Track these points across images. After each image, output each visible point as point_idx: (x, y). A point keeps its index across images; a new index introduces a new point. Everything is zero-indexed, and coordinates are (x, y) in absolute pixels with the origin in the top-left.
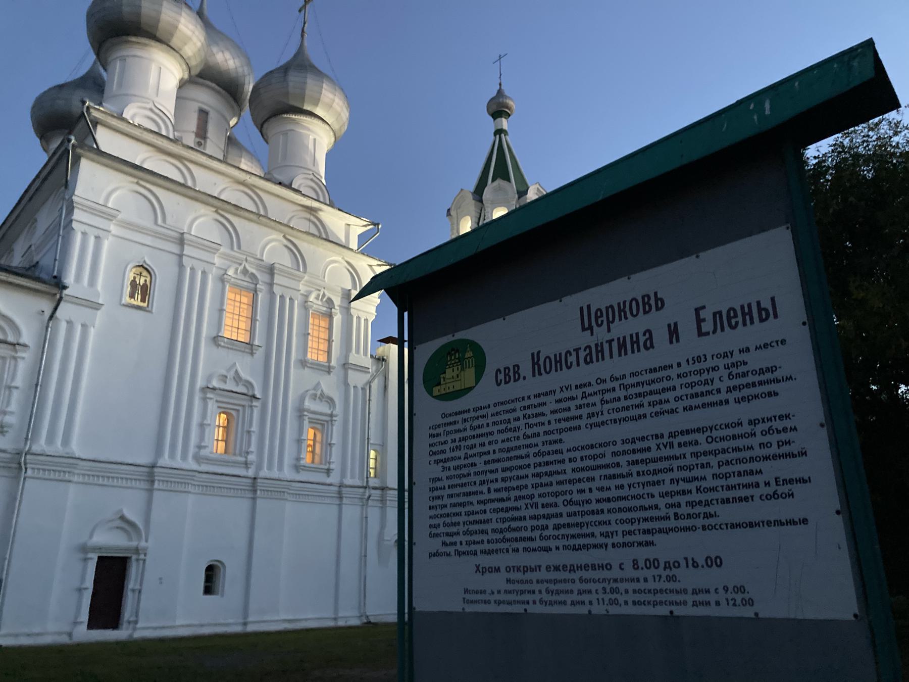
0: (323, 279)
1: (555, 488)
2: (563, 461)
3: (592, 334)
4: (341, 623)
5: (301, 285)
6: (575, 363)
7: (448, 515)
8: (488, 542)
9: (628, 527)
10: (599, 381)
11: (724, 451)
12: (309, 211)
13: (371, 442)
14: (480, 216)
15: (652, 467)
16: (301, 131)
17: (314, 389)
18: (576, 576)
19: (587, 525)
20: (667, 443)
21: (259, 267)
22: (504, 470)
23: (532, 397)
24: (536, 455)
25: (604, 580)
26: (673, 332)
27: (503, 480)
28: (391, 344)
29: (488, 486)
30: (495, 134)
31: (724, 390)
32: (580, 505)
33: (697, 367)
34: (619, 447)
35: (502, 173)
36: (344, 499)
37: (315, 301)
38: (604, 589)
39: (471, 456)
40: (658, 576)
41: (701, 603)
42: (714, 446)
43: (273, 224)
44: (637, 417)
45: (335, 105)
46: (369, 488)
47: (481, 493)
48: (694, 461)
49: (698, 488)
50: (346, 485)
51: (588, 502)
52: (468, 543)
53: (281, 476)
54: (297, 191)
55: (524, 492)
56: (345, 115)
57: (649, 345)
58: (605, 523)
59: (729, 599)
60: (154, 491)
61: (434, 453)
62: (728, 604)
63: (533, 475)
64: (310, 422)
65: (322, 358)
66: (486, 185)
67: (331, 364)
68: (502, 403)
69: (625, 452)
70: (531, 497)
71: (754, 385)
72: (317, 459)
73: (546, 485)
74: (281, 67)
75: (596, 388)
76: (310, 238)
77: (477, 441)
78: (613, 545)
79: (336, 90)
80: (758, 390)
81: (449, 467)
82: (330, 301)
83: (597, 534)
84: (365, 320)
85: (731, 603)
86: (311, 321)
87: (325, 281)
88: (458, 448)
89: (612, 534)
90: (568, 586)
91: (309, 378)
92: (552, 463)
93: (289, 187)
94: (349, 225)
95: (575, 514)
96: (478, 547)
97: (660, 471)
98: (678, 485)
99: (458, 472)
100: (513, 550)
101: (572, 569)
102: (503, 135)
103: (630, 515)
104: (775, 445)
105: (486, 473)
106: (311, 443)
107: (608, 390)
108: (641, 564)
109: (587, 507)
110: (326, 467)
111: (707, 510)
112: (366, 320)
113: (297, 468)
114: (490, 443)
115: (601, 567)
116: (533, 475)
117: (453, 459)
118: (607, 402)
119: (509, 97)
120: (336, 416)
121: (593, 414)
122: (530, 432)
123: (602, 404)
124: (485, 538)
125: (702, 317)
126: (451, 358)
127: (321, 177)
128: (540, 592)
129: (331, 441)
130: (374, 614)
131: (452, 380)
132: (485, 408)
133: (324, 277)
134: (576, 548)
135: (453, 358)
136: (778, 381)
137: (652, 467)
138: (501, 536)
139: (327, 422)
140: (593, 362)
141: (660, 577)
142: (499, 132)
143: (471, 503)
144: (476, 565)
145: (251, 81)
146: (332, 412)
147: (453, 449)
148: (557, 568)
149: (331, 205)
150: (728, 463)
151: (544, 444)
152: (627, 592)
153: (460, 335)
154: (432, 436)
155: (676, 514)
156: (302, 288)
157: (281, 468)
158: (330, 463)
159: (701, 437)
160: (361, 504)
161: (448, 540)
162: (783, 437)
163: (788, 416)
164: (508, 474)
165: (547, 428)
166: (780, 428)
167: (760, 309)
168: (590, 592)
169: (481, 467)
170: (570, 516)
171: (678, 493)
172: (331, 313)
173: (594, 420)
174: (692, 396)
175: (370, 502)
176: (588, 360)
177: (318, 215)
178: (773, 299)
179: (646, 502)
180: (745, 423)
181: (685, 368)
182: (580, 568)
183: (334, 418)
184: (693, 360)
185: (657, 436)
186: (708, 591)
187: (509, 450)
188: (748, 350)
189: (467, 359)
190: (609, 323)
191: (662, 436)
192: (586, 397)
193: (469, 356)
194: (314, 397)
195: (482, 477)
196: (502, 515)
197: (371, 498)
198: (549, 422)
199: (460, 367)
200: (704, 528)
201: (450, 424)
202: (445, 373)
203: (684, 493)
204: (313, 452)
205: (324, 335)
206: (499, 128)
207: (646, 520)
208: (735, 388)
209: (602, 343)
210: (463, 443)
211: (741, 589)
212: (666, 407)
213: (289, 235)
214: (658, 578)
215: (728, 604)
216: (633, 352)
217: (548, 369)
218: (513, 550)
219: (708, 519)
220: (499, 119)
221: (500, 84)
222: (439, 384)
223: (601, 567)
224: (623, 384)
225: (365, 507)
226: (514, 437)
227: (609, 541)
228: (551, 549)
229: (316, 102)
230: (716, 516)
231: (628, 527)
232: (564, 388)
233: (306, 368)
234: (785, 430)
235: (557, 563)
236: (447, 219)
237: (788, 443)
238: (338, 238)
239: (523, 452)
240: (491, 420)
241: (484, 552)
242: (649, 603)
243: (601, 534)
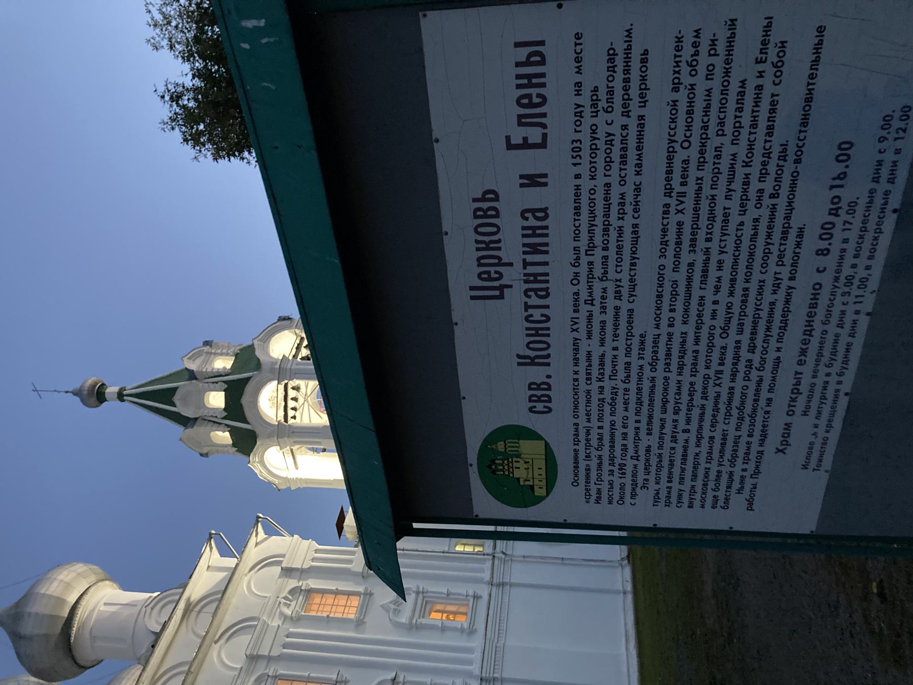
0: (268, 599)
1: (702, 347)
2: (670, 335)
3: (510, 286)
4: (629, 587)
5: (273, 624)
6: (545, 311)
7: (705, 485)
8: (750, 436)
9: (773, 258)
10: (575, 282)
11: (705, 128)
12: (189, 612)
13: (446, 549)
14: (211, 421)
15: (703, 222)
16: (93, 619)
17: (388, 611)
18: (817, 326)
19: (759, 310)
20: (677, 200)
21: (249, 673)
22: (664, 411)
23: (576, 369)
24: (653, 369)
25: (833, 294)
26: (532, 181)
27: (676, 412)
28: (345, 524)
29: (681, 432)
30: (123, 401)
31: (625, 121)
32: (730, 318)
33: (586, 152)
34: (669, 261)
35: (167, 396)
36: (504, 580)
37: (292, 607)
38: (843, 294)
39: (636, 452)
40: (844, 225)
41: (892, 172)
42: (695, 140)
43: (200, 655)
44: (634, 236)
45: (67, 579)
46: (494, 553)
47: (687, 441)
48: (709, 167)
49: (744, 164)
50: (491, 578)
51: (729, 307)
52: (746, 461)
53: (480, 650)
54: (165, 626)
55: (699, 387)
56: (80, 567)
57: (542, 213)
58: (761, 287)
59: (897, 136)
60: (503, 676)
61: (622, 498)
62: (903, 138)
63: (680, 374)
64: (423, 617)
65: (355, 601)
66: (179, 413)
67: (363, 592)
68: (576, 407)
69: (677, 255)
70: (706, 378)
71: (627, 81)
72: (462, 610)
73: (696, 358)
74: (13, 642)
75: (583, 288)
76: (220, 612)
77: (619, 442)
78: (792, 279)
79: (49, 578)
80: (635, 75)
81: (645, 480)
82: (293, 592)
83: (772, 298)
84: (316, 553)
85: (901, 134)
86: (313, 614)
87: (270, 597)
88: (622, 467)
89: (778, 279)
90: (830, 338)
91: (376, 616)
92: (669, 349)
93: (158, 636)
94: (209, 567)
95: (741, 324)
96: (755, 448)
97: (712, 211)
98: (734, 191)
99: (653, 469)
100: (768, 405)
101: (809, 332)
102: (125, 393)
103: (759, 254)
104: (713, 60)
105: (663, 434)
106: (445, 615)
107: (591, 270)
108: (823, 245)
109: (736, 310)
110: (472, 600)
111: (775, 156)
112: (317, 551)
113: (471, 632)
114: (625, 426)
115: (815, 297)
116: (680, 374)
117: (634, 475)
118: (606, 272)
119: (83, 383)
120: (418, 587)
121: (616, 292)
122: (621, 375)
123: (607, 280)
124: (745, 439)
125: (521, 142)
126: (500, 470)
127: (150, 597)
128: (828, 375)
129: (445, 594)
130: (619, 551)
131: (530, 471)
132: (577, 430)
133: (266, 597)
134: (784, 327)
135: (501, 467)
136: (629, 48)
137: (703, 222)
138: (747, 419)
139: (424, 598)
140: (548, 288)
141: (845, 222)
142: (121, 396)
143: (697, 454)
144: (776, 453)
145: (26, 678)
146: (414, 592)
147: (622, 474)
148: (803, 352)
149: (184, 586)
150: (722, 123)
151: (641, 358)
152: (854, 266)
153: (472, 456)
154: (598, 501)
155: (772, 196)
156: (276, 622)
157: (470, 650)
158: (467, 596)
159: (681, 155)
160: (510, 562)
161: (736, 485)
162: (704, 48)
163: (679, 40)
164: (670, 407)
165: (621, 352)
166: (693, 51)
167: (527, 63)
168: (843, 312)
169: (654, 440)
170: (742, 331)
171: (745, 191)
172: (305, 590)
173: (625, 292)
174: (623, 162)
175: (508, 552)
176: (544, 293)
177: (194, 603)
178: (518, 45)
179: (748, 231)
180: (675, 96)
181: (584, 170)
182: (809, 323)
183: (421, 590)
184: (575, 158)
185: (665, 213)
186: (880, 163)
187: (639, 402)
188: (578, 84)
189: (506, 449)
190: (500, 264)
191: (667, 205)
192: (592, 300)
193: (503, 446)
194: (397, 612)
195: (667, 438)
196: (720, 417)
197: (504, 551)
198: (616, 349)
199: (515, 459)
200: (798, 161)
201: (588, 476)
202: (518, 479)
203: (746, 183)
204: (455, 613)
205: (330, 599)
206: (116, 396)
207: (769, 236)
208: (625, 106)
209: (525, 275)
210: (618, 461)
211: (887, 120)
212: (630, 198)
213: (215, 636)
214: (847, 224)
215: (903, 138)
216: (546, 235)
217: (545, 346)
218: (768, 405)
219: (787, 155)
220: (106, 396)
221: (67, 392)
222: (532, 487)
223: (815, 297)
224: (586, 251)
225: (513, 558)
226: (624, 394)
227: (785, 283)
228: (779, 358)
229: (61, 601)
230: (786, 145)
231: (773, 258)
232: (575, 327)
233: (365, 620)
234: (695, 45)
235: (797, 351)
236: (211, 457)
237: (713, 42)
238: (222, 580)
239: (646, 385)
240: (595, 423)
241: (762, 443)
242: (876, 239)
243: (775, 292)
